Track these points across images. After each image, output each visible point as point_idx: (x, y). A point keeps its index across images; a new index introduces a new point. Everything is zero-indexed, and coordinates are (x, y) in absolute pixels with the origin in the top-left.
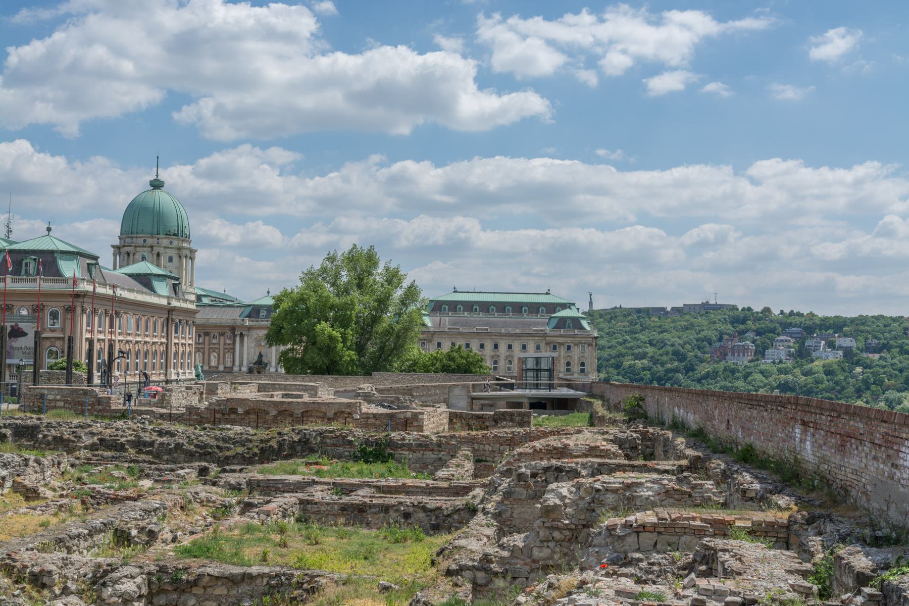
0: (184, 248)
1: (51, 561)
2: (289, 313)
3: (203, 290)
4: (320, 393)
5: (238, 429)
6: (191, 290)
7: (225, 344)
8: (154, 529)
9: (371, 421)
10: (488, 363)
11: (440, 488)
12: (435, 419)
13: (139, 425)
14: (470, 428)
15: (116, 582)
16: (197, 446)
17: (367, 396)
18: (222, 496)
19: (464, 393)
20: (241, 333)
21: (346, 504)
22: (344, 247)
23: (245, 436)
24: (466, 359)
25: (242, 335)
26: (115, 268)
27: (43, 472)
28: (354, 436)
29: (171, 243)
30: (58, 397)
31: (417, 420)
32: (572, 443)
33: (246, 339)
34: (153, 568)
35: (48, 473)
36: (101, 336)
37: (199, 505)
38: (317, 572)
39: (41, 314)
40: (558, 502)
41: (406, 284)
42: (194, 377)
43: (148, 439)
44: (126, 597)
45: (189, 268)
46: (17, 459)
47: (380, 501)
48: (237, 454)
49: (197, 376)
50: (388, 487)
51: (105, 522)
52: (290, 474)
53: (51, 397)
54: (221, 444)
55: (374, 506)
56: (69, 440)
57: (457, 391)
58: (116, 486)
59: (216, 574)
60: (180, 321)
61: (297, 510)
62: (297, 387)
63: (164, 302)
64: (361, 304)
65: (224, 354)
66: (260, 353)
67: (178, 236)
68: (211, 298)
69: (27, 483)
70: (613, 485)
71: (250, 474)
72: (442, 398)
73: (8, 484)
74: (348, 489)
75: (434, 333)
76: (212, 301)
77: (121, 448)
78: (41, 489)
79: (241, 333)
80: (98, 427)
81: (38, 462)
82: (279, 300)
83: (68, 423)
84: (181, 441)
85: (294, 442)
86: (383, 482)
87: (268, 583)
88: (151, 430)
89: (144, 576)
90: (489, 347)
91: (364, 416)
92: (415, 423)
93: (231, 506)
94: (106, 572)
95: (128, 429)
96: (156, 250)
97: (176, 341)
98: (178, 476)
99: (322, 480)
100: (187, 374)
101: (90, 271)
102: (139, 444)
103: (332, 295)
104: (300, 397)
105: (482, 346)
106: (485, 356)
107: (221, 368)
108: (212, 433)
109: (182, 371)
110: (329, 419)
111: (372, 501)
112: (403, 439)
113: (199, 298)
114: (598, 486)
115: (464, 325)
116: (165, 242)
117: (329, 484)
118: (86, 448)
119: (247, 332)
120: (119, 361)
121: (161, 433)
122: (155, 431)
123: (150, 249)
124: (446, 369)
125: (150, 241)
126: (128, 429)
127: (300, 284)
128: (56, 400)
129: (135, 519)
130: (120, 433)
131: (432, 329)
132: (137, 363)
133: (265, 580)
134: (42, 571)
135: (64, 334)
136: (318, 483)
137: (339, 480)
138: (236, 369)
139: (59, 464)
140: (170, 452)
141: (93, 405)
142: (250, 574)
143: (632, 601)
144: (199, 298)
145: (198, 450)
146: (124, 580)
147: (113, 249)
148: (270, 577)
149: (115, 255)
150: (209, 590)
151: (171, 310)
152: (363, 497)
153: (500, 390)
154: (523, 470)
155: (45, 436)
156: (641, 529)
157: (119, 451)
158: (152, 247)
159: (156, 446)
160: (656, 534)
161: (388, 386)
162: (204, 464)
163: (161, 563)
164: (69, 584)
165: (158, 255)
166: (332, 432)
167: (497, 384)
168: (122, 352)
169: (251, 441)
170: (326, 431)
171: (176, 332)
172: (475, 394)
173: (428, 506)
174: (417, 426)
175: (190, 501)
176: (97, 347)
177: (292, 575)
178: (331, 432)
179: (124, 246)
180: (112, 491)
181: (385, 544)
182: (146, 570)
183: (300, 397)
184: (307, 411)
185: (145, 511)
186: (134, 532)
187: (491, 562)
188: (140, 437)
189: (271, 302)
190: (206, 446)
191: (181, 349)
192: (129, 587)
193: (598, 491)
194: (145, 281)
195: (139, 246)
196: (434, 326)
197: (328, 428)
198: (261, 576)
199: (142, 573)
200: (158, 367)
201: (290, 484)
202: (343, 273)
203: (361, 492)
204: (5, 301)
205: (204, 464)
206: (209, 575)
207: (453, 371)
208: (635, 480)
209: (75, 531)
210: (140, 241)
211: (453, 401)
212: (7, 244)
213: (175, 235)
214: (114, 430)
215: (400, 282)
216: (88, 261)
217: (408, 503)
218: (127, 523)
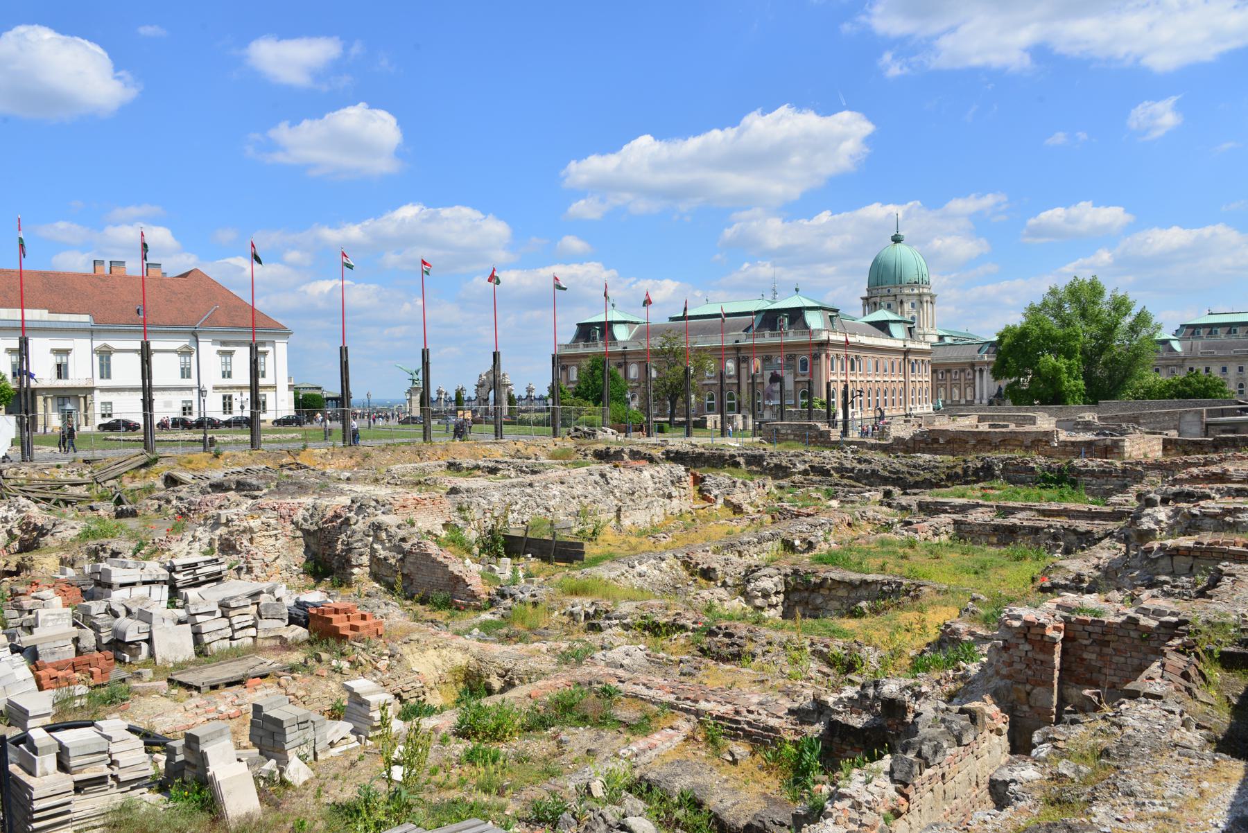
0: (925, 294)
1: (716, 562)
2: (1012, 349)
5: (927, 457)
6: (933, 332)
7: (965, 379)
9: (1068, 449)
10: (1232, 387)
11: (1103, 513)
14: (1186, 453)
16: (890, 472)
18: (887, 515)
19: (1196, 418)
21: (998, 525)
22: (1062, 284)
23: (932, 463)
24: (1204, 383)
25: (981, 371)
26: (865, 315)
27: (748, 492)
28: (1036, 463)
32: (1231, 469)
34: (789, 571)
35: (753, 493)
37: (865, 523)
38: (925, 581)
40: (1153, 526)
41: (1135, 311)
42: (931, 410)
43: (849, 466)
46: (727, 481)
48: (926, 479)
50: (1050, 510)
52: (959, 497)
53: (783, 431)
54: (912, 470)
55: (1024, 527)
56: (787, 467)
57: (1188, 418)
58: (800, 504)
59: (837, 579)
61: (951, 529)
62: (1004, 418)
63: (900, 344)
64: (1084, 333)
65: (951, 389)
69: (734, 500)
70: (1212, 510)
71: (922, 497)
73: (720, 501)
74: (1006, 512)
75: (1184, 359)
77: (826, 473)
80: (809, 456)
82: (1002, 336)
83: (786, 453)
84: (877, 468)
85: (977, 468)
86: (1045, 506)
87: (881, 589)
90: (1233, 370)
92: (1116, 450)
93: (893, 524)
94: (754, 571)
97: (913, 379)
98: (864, 497)
99: (986, 503)
101: (831, 321)
102: (841, 470)
103: (1055, 328)
104: (1006, 426)
105: (1224, 369)
106: (1228, 379)
107: (963, 401)
108: (903, 461)
110: (1027, 447)
112: (1086, 466)
113: (941, 338)
114: (1195, 511)
115: (1220, 347)
116: (907, 291)
117: (992, 506)
118: (799, 473)
121: (860, 461)
124: (1182, 395)
125: (893, 291)
128: (788, 434)
130: (826, 461)
131: (1182, 355)
133: (879, 586)
134: (709, 568)
136: (982, 506)
137: (1002, 503)
138: (977, 402)
139: (764, 486)
140: (867, 477)
141: (816, 437)
142: (865, 581)
143: (1066, 614)
145: (892, 475)
146: (763, 578)
148: (883, 584)
149: (864, 306)
150: (834, 592)
151: (907, 352)
153: (1241, 415)
154: (1152, 495)
155: (768, 464)
156: (1175, 553)
158: (895, 296)
160: (1191, 558)
162: (891, 488)
163: (795, 567)
164: (727, 580)
165: (902, 302)
166: (1015, 459)
167: (1240, 409)
169: (938, 467)
170: (1008, 458)
172: (1210, 419)
173: (1079, 529)
175: (857, 519)
177: (902, 583)
178: (1012, 459)
180: (796, 509)
181: (1005, 561)
182: (783, 572)
183: (1006, 426)
185: (811, 525)
186: (797, 542)
188: (842, 464)
189: (996, 339)
190: (898, 472)
191: (918, 386)
193: (1195, 515)
194: (883, 326)
196: (1184, 351)
197: (1010, 456)
198: (875, 582)
201: (956, 506)
202: (1066, 306)
203: (1020, 515)
207: (1190, 397)
208: (1238, 506)
209: (746, 539)
210: (885, 291)
211: (1184, 427)
215: (1129, 309)
216: (830, 314)
218: (792, 534)
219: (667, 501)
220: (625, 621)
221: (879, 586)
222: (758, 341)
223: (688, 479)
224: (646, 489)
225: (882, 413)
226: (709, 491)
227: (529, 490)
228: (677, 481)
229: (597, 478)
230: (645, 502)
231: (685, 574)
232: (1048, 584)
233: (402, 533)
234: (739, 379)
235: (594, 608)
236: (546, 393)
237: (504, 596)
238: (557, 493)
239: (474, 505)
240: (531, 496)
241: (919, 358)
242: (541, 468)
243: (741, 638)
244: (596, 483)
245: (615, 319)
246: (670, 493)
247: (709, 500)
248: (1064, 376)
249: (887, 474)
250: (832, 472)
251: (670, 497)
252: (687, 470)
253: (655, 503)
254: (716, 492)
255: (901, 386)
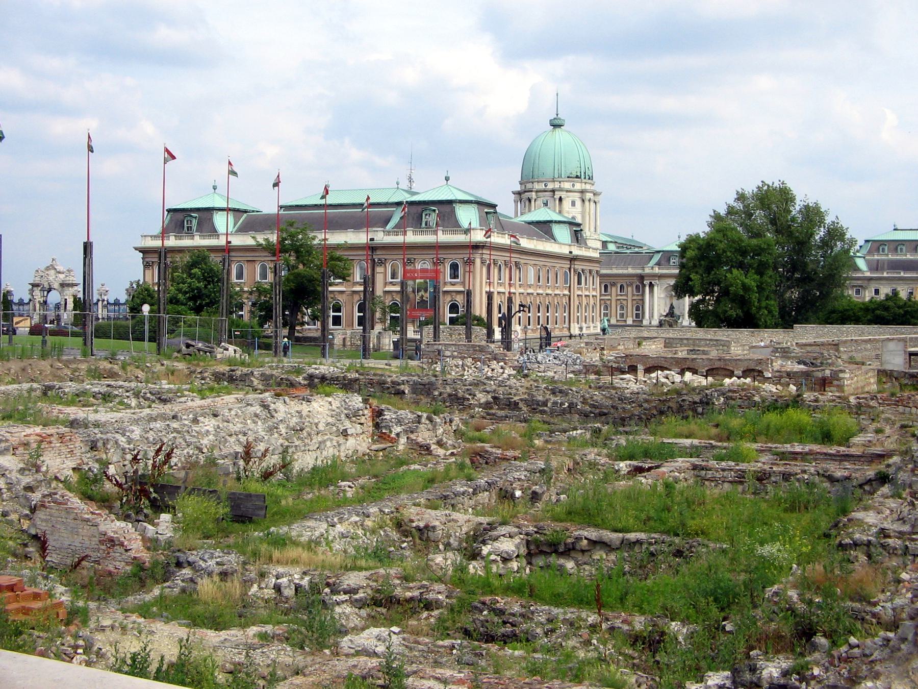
3: (609, 236)
4: (733, 348)
6: (596, 237)
7: (633, 295)
8: (537, 490)
12: (859, 378)
13: (532, 382)
15: (496, 539)
16: (593, 406)
17: (786, 352)
20: (651, 283)
25: (651, 285)
27: (434, 429)
29: (573, 185)
30: (456, 353)
31: (837, 380)
33: (656, 288)
36: (501, 290)
39: (472, 266)
43: (540, 398)
44: (505, 555)
45: (593, 211)
46: (410, 416)
47: (782, 469)
49: (604, 330)
51: (489, 481)
60: (583, 270)
63: (565, 250)
66: (672, 305)
67: (580, 178)
68: (617, 245)
72: (874, 354)
73: (403, 440)
76: (618, 247)
77: (514, 406)
78: (433, 447)
79: (651, 283)
81: (430, 419)
88: (545, 388)
89: (522, 536)
91: (777, 374)
92: (835, 383)
95: (521, 387)
96: (557, 196)
97: (580, 293)
100: (592, 328)
109: (586, 325)
111: (772, 468)
113: (605, 244)
116: (567, 185)
118: (480, 406)
119: (657, 281)
120: (520, 315)
122: (548, 389)
123: (552, 193)
126: (521, 387)
127: (707, 229)
129: (519, 480)
130: (514, 391)
132: (548, 317)
135: (464, 287)
139: (451, 421)
144: (605, 244)
147: (513, 196)
151: (573, 259)
152: (764, 463)
157: (513, 410)
159: (549, 404)
161: (811, 340)
162: (598, 425)
165: (560, 199)
168: (523, 306)
171: (579, 283)
174: (838, 386)
176: (496, 301)
179: (525, 192)
184: (713, 369)
187: (887, 536)
188: (533, 396)
192: (508, 546)
195: (541, 191)
199: (521, 534)
200: (534, 321)
204: (437, 254)
205: (598, 425)
206: (586, 538)
212: (409, 196)
213: (577, 177)
214: (507, 388)
217: (812, 471)
219: (341, 439)
220: (357, 596)
221: (644, 546)
222: (399, 239)
223: (366, 412)
224: (317, 424)
225: (549, 334)
226: (389, 428)
227: (175, 425)
228: (353, 415)
229: (257, 409)
230: (317, 439)
231: (395, 535)
232: (848, 541)
233: (27, 480)
234: (570, 291)
235: (307, 578)
236: (123, 298)
237: (179, 565)
238: (211, 429)
239: (111, 443)
240: (178, 432)
241: (587, 266)
242: (171, 395)
243: (514, 615)
244: (256, 415)
245: (217, 205)
246: (345, 430)
247: (392, 441)
248: (755, 297)
249: (588, 408)
250: (521, 405)
251: (345, 434)
252: (365, 401)
253: (328, 444)
254: (399, 429)
255: (565, 301)
